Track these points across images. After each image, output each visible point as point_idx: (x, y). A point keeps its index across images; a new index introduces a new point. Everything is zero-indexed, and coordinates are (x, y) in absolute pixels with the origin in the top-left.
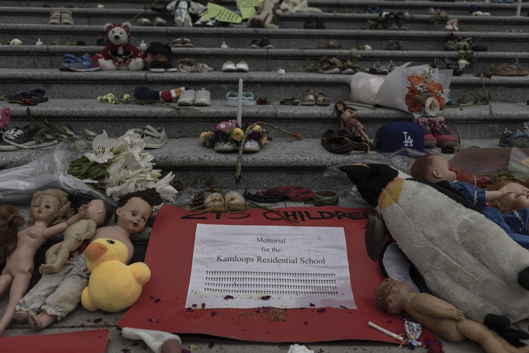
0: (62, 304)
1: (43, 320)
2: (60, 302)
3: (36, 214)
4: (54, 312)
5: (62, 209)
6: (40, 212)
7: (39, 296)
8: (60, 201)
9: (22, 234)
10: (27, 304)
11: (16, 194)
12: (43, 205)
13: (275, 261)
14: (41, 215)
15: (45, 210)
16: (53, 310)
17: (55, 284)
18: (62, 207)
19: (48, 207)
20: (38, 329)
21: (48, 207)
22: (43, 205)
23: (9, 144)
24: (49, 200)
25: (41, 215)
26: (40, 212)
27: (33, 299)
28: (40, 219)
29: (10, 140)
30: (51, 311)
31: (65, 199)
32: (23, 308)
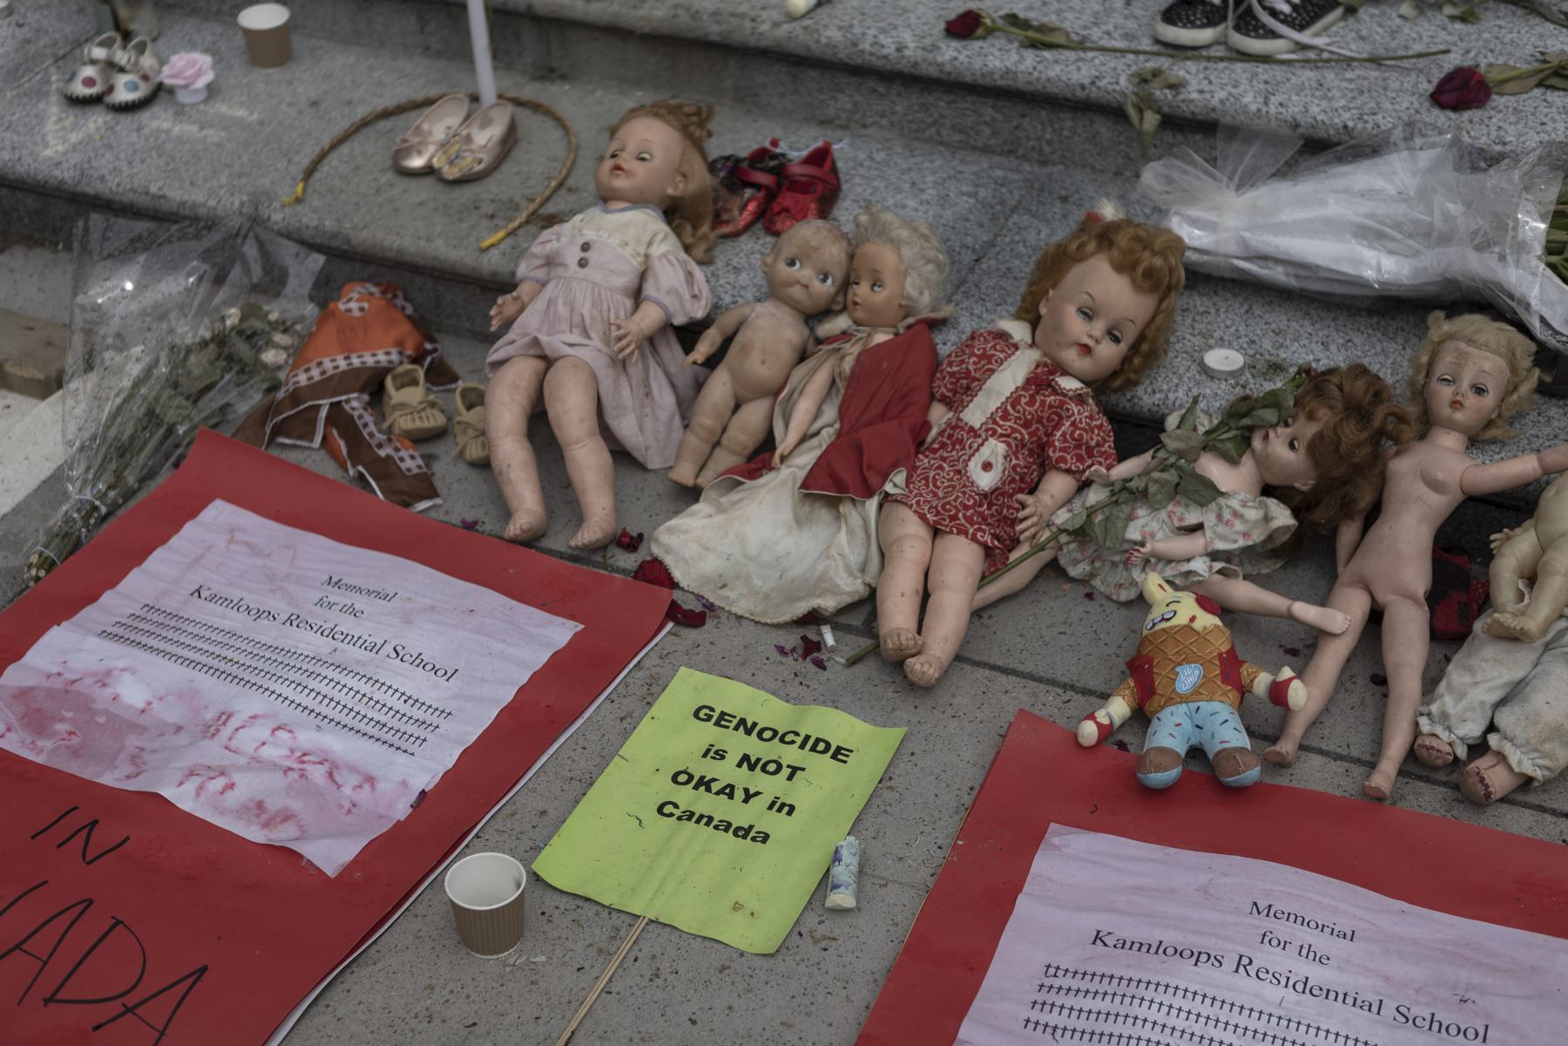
0: (1547, 746)
1: (1499, 780)
2: (287, 235)
3: (1444, 410)
4: (1528, 768)
5: (1515, 396)
6: (1456, 404)
7: (1482, 703)
8: (1514, 369)
9: (1404, 467)
10: (1453, 720)
11: (1338, 281)
12: (1465, 384)
13: (1300, 987)
14: (1459, 416)
15: (1471, 400)
16: (1525, 759)
17: (1518, 674)
18: (1516, 388)
19: (1480, 390)
20: (1480, 801)
21: (1480, 390)
22: (1465, 384)
23: (1273, 35)
24: (1487, 366)
25: (1459, 416)
26: (1456, 404)
27: (1466, 710)
28: (1451, 426)
29: (1274, 13)
30: (1520, 762)
31: (1526, 363)
32: (1439, 730)
